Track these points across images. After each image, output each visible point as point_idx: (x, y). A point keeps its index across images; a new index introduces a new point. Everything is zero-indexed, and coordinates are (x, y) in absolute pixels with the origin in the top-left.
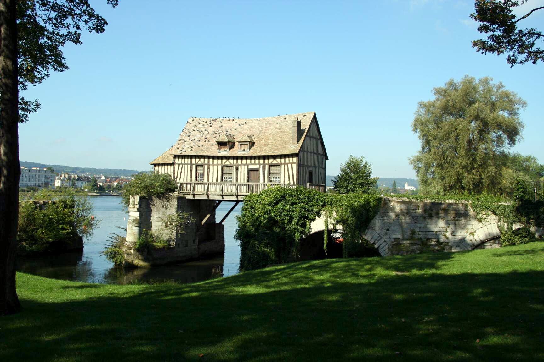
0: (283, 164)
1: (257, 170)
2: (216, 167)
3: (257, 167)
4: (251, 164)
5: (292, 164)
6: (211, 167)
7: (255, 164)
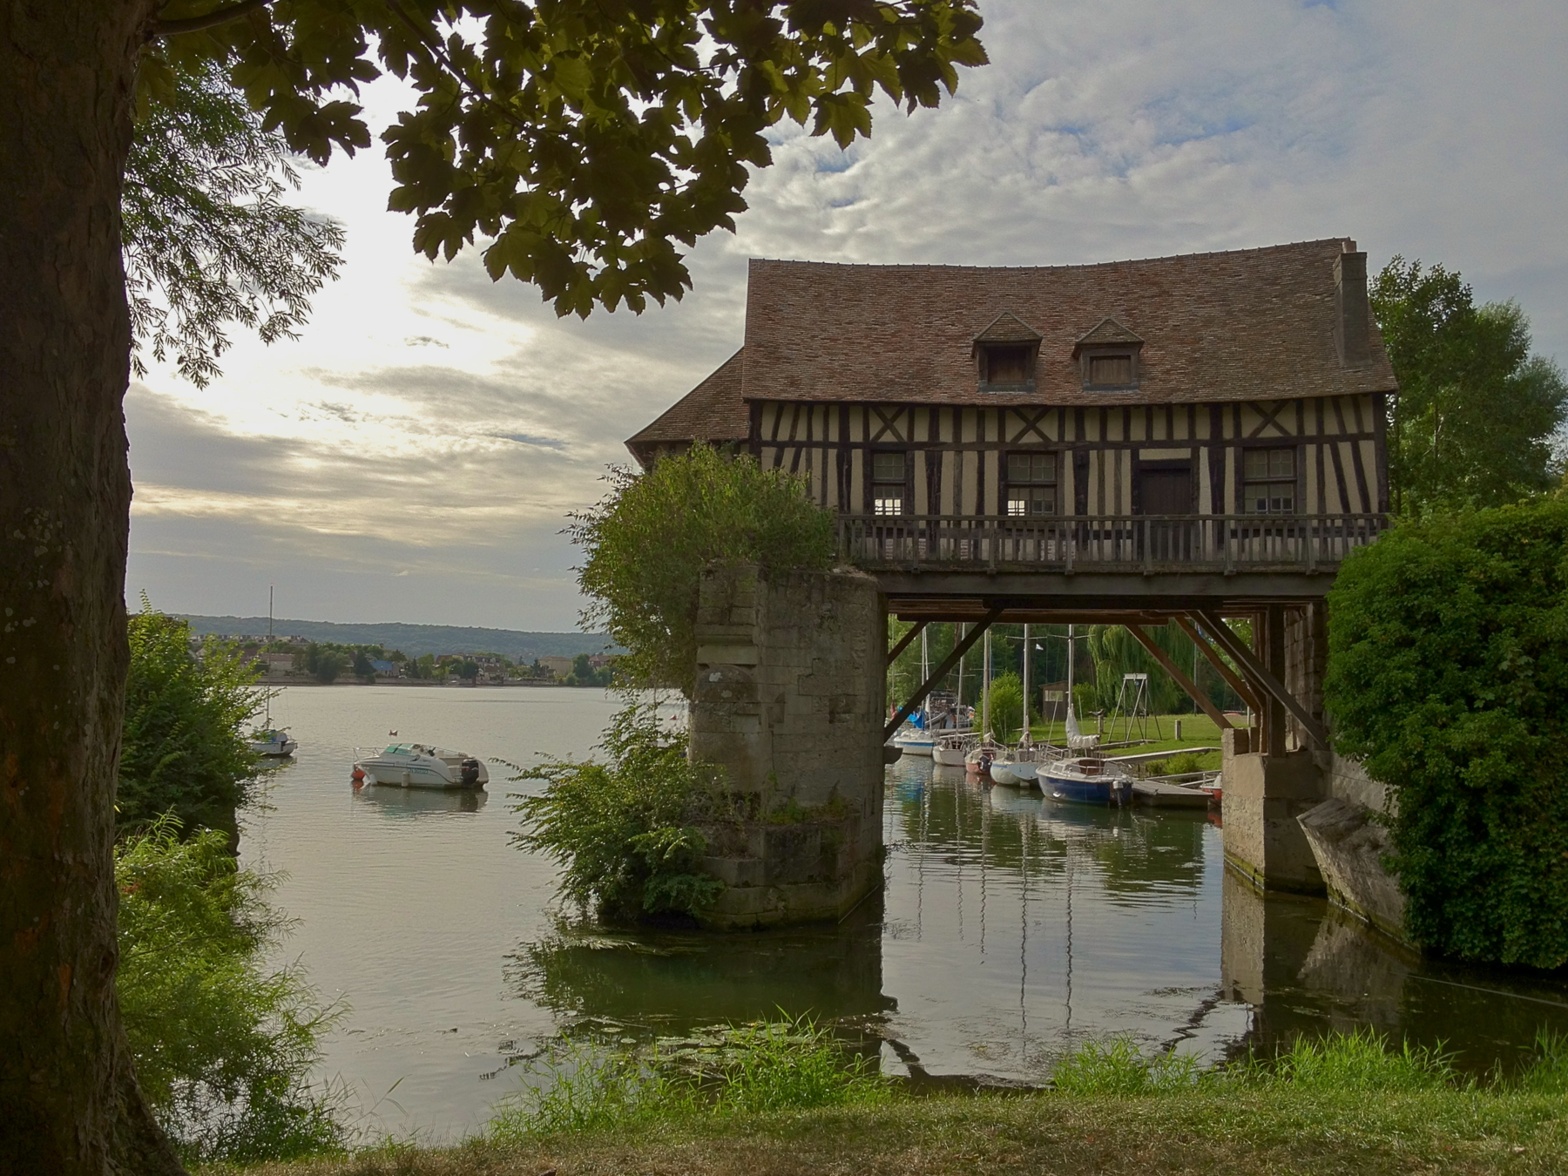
0: (1311, 440)
1: (1185, 470)
2: (971, 457)
3: (1184, 454)
4: (1151, 443)
5: (1355, 440)
6: (948, 457)
7: (1169, 443)
